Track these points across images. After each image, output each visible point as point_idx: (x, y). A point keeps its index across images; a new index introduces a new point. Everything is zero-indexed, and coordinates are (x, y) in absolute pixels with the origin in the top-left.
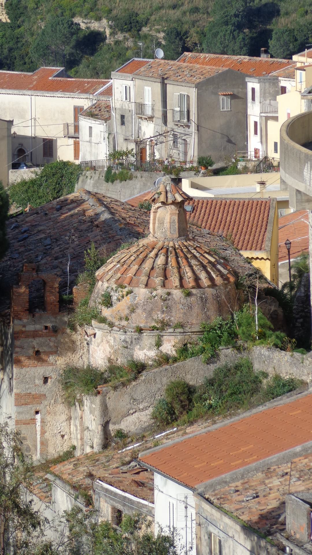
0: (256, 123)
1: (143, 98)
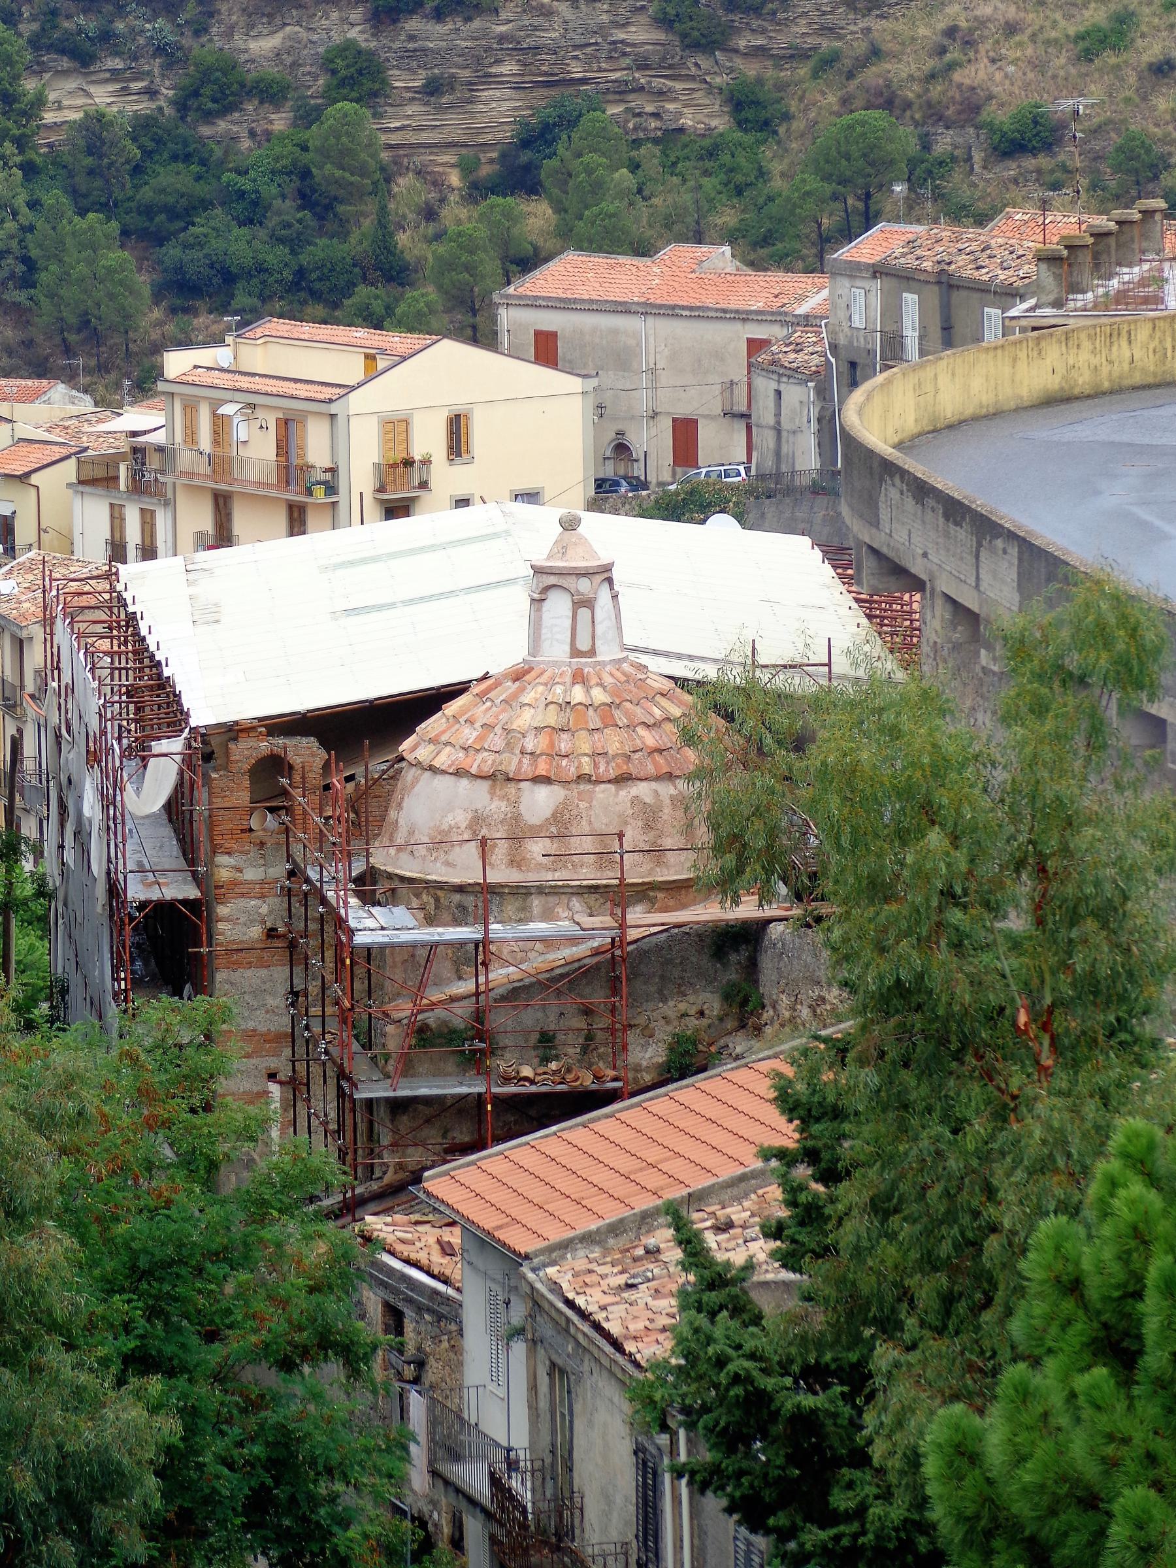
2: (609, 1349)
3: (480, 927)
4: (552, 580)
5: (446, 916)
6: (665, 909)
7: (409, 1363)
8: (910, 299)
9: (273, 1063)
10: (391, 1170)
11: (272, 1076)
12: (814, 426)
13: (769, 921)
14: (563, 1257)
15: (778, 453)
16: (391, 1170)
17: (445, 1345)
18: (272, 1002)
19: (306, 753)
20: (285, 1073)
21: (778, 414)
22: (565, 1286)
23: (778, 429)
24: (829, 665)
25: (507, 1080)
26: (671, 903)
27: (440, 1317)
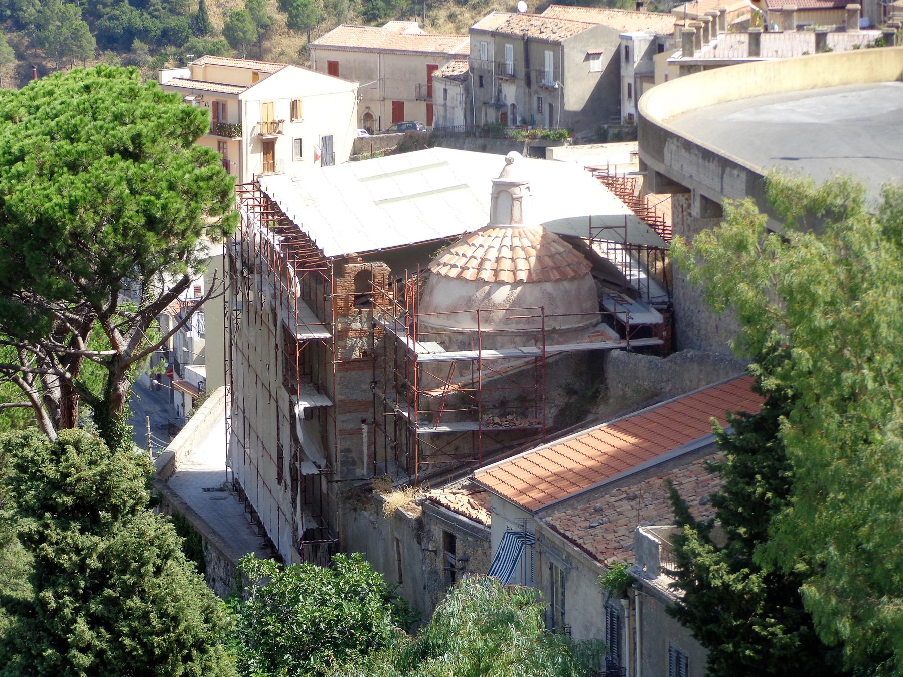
0: (629, 85)
1: (503, 56)
2: (589, 557)
3: (477, 352)
4: (503, 188)
5: (455, 347)
6: (558, 343)
7: (459, 560)
8: (509, 47)
9: (364, 415)
10: (430, 467)
11: (363, 421)
12: (463, 105)
13: (612, 349)
14: (553, 512)
15: (445, 118)
16: (430, 467)
17: (480, 552)
18: (364, 387)
19: (381, 268)
20: (370, 419)
21: (445, 99)
22: (558, 527)
23: (445, 105)
24: (625, 227)
25: (488, 424)
26: (561, 340)
27: (477, 539)
